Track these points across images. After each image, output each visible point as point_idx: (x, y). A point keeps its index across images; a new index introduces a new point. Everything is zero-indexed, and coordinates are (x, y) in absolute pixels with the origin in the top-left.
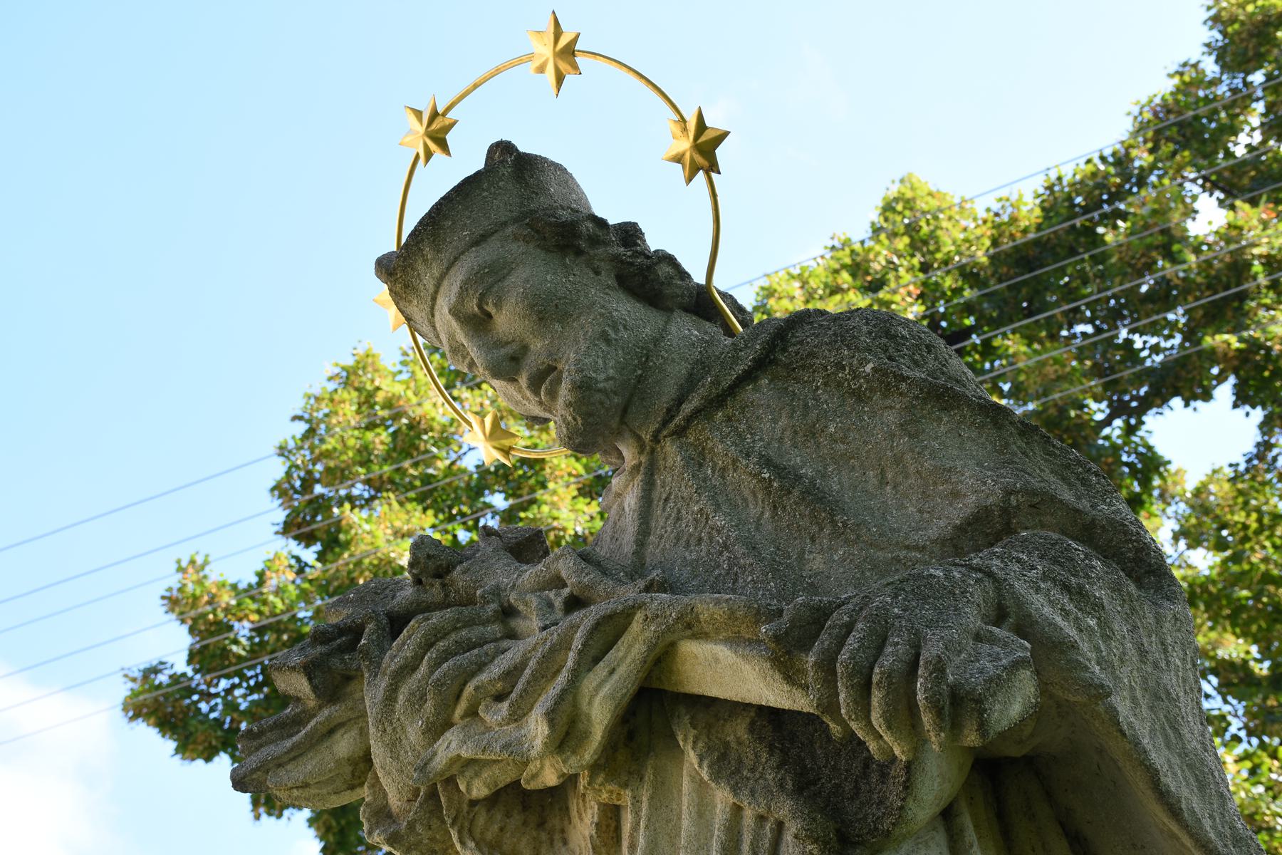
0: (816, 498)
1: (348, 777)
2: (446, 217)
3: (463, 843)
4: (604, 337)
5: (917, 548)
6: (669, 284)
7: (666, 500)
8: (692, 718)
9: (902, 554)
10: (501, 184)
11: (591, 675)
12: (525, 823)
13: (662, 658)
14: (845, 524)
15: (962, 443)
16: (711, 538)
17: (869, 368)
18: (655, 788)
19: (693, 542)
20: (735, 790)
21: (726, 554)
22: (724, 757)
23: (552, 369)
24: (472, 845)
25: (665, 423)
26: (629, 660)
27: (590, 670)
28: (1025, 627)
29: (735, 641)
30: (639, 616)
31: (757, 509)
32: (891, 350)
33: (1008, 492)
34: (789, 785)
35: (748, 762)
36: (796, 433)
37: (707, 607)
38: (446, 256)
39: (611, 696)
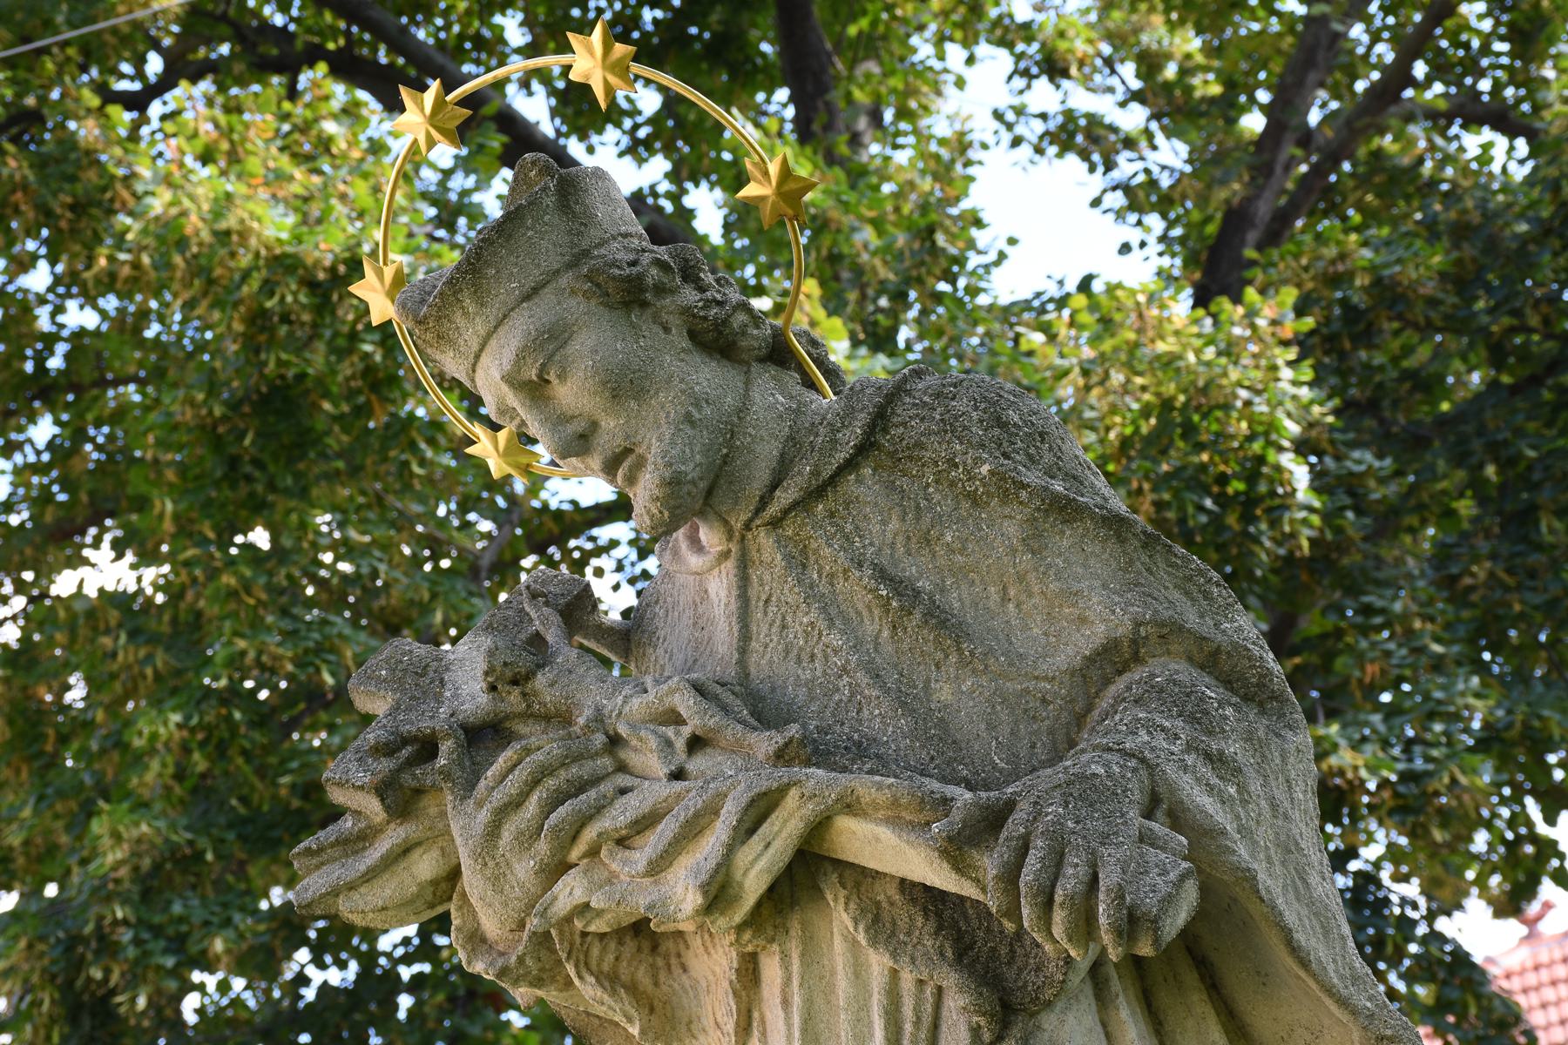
0: (940, 620)
2: (488, 264)
3: (581, 977)
5: (1046, 678)
6: (744, 333)
7: (767, 601)
9: (1031, 685)
11: (745, 848)
12: (639, 950)
13: (819, 828)
14: (972, 653)
16: (826, 657)
17: (985, 469)
18: (804, 943)
19: (805, 657)
20: (894, 955)
21: (846, 679)
22: (877, 919)
23: (628, 451)
25: (758, 511)
28: (1178, 818)
29: (894, 822)
30: (794, 793)
31: (873, 625)
33: (1138, 624)
34: (949, 954)
35: (902, 924)
37: (866, 786)
38: (493, 312)
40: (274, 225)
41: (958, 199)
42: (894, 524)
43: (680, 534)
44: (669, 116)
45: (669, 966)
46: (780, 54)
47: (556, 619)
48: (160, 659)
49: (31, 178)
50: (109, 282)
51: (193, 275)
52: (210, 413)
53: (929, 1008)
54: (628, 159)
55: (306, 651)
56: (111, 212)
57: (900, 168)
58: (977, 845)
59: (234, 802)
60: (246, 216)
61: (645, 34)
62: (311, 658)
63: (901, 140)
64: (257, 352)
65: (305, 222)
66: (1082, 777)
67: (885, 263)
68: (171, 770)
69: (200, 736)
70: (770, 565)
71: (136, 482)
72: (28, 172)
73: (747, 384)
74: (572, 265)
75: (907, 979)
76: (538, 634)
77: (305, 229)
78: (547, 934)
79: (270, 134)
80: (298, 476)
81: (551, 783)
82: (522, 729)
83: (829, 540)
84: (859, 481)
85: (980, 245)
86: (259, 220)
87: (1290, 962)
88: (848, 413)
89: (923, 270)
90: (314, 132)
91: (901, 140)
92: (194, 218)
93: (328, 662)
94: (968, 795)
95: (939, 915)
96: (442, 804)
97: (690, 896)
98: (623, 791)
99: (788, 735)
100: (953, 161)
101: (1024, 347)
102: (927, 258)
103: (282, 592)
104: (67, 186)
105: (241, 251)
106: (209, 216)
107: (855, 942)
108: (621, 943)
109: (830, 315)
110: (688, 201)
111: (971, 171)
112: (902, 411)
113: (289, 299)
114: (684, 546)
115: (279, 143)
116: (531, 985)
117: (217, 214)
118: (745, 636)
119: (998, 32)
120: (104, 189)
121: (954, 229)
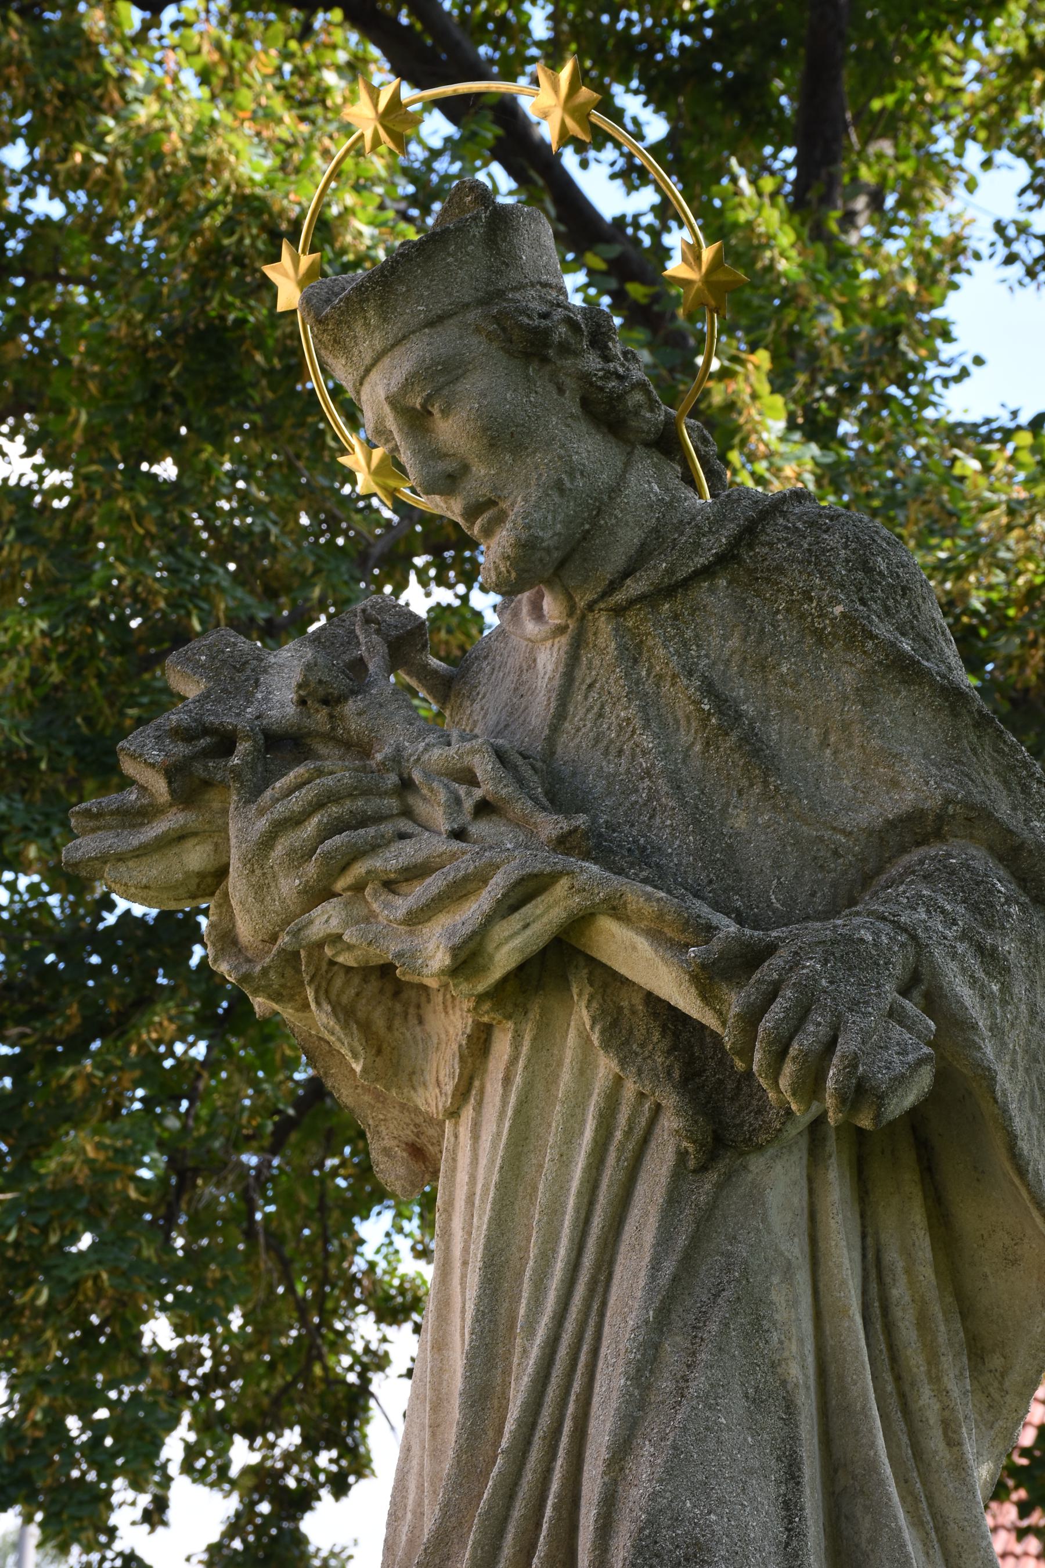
0: (755, 749)
1: (193, 888)
3: (318, 1003)
4: (559, 487)
5: (843, 832)
6: (637, 414)
7: (591, 686)
8: (591, 973)
9: (827, 834)
10: (470, 248)
11: (504, 923)
12: (381, 991)
13: (580, 922)
14: (777, 788)
15: (914, 724)
16: (633, 756)
17: (838, 609)
19: (613, 751)
20: (623, 1063)
22: (615, 1023)
23: (491, 503)
24: (329, 1008)
25: (605, 595)
26: (545, 920)
27: (503, 917)
28: (935, 1002)
29: (655, 935)
32: (865, 590)
33: (947, 801)
34: (676, 1074)
35: (639, 1034)
36: (745, 659)
37: (637, 895)
38: (394, 329)
39: (521, 950)
40: (251, 164)
41: (932, 306)
42: (734, 642)
43: (525, 597)
44: (671, 150)
45: (406, 1014)
46: (797, 113)
47: (383, 649)
48: (42, 564)
49: (29, 55)
50: (81, 178)
51: (160, 194)
52: (145, 335)
53: (643, 1121)
54: (619, 182)
55: (181, 593)
56: (98, 110)
57: (888, 259)
58: (728, 979)
59: (79, 720)
60: (225, 147)
61: (668, 57)
62: (185, 601)
63: (896, 229)
64: (204, 287)
65: (283, 166)
66: (849, 940)
67: (842, 352)
68: (26, 673)
69: (61, 649)
70: (602, 652)
71: (58, 386)
72: (26, 47)
73: (627, 465)
74: (481, 302)
75: (630, 1089)
76: (361, 659)
77: (280, 175)
78: (296, 954)
79: (270, 70)
80: (214, 420)
81: (334, 809)
82: (322, 749)
83: (667, 640)
84: (712, 590)
85: (944, 356)
86: (237, 155)
87: (1008, 1166)
88: (719, 519)
89: (878, 369)
90: (314, 79)
91: (896, 229)
92: (175, 136)
93: (201, 609)
94: (733, 928)
95: (676, 1035)
96: (226, 801)
97: (439, 955)
98: (402, 836)
99: (574, 823)
100: (941, 264)
101: (957, 471)
102: (886, 359)
103: (174, 529)
104: (61, 72)
105: (213, 181)
106: (189, 138)
107: (588, 1040)
108: (365, 980)
109: (773, 392)
110: (667, 240)
111: (958, 278)
112: (771, 532)
113: (247, 241)
114: (525, 609)
115: (277, 81)
116: (270, 997)
117: (197, 139)
118: (561, 714)
119: (1023, 142)
120: (97, 85)
121: (920, 336)
